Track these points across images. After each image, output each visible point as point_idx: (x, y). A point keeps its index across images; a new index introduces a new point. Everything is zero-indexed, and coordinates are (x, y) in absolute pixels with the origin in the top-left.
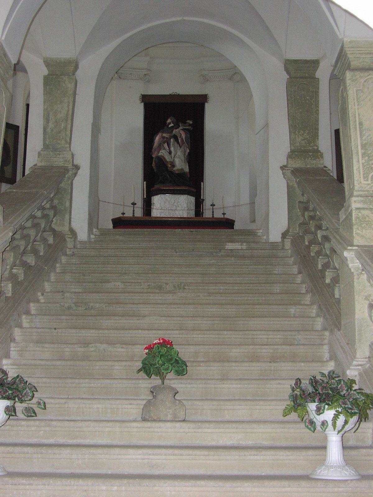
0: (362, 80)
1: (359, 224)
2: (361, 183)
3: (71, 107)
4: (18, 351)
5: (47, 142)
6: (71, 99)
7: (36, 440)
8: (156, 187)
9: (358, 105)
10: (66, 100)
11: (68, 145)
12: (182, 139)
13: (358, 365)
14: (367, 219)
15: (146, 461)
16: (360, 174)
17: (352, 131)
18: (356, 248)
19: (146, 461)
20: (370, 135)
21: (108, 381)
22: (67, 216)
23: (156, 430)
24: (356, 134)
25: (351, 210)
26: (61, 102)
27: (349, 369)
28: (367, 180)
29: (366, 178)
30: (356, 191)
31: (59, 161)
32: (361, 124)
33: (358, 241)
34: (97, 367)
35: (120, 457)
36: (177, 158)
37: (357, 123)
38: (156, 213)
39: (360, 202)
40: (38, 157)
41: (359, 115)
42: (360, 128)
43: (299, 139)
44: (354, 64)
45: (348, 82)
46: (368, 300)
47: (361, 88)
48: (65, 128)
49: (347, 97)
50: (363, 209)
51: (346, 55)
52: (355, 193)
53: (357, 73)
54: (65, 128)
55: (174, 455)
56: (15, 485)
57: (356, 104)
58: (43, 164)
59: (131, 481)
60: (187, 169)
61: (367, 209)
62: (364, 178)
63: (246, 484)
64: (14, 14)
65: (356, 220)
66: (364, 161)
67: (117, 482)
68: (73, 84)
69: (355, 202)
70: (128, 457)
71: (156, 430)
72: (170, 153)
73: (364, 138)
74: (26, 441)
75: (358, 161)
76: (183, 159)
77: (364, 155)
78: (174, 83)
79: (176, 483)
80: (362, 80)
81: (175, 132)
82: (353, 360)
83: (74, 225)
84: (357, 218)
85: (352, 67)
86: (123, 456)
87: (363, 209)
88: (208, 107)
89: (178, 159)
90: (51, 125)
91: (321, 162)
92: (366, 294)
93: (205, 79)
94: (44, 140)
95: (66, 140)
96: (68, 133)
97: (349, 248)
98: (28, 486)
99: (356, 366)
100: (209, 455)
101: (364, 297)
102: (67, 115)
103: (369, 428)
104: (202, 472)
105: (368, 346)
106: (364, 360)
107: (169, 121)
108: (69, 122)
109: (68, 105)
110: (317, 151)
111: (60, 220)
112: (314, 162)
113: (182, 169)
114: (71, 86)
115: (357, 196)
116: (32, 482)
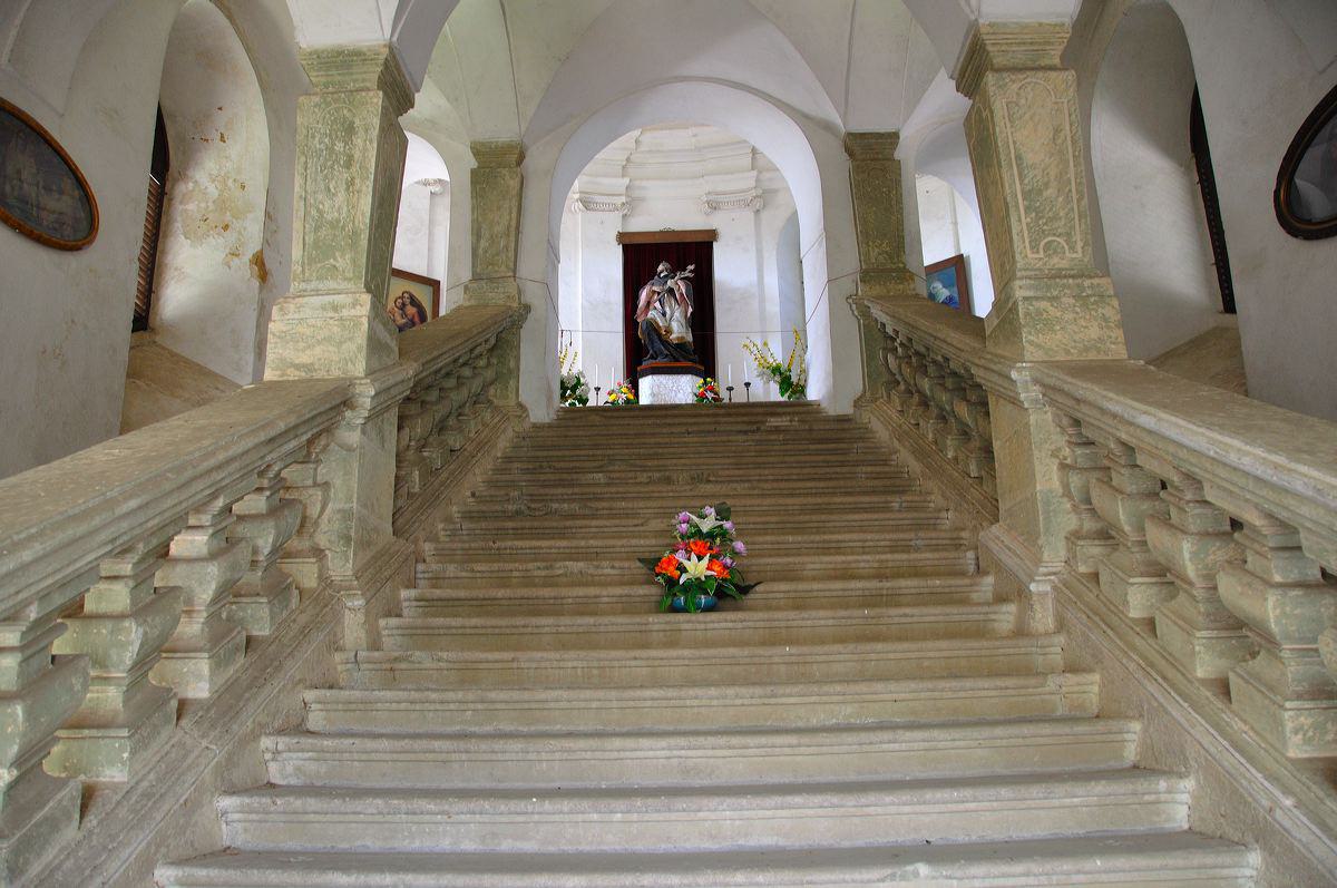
0: (1015, 87)
1: (1031, 324)
2: (1026, 256)
3: (514, 215)
4: (428, 579)
5: (478, 270)
6: (514, 203)
7: (458, 728)
8: (646, 364)
9: (1012, 126)
10: (506, 206)
11: (511, 274)
12: (682, 295)
13: (1050, 574)
14: (1045, 315)
15: (675, 761)
16: (1024, 242)
17: (1004, 170)
18: (1029, 365)
19: (675, 761)
20: (1035, 176)
21: (591, 620)
22: (512, 383)
23: (688, 702)
24: (1012, 175)
25: (1015, 303)
26: (499, 208)
27: (1034, 581)
28: (1038, 252)
29: (1035, 249)
30: (1020, 270)
31: (497, 297)
32: (1019, 158)
33: (1031, 353)
34: (570, 601)
35: (622, 755)
36: (675, 322)
37: (1013, 157)
38: (644, 400)
39: (1030, 287)
40: (465, 293)
41: (1014, 142)
42: (1018, 166)
43: (873, 254)
44: (998, 61)
45: (991, 90)
46: (1058, 457)
47: (1014, 100)
48: (506, 247)
49: (992, 117)
50: (1037, 298)
51: (983, 46)
52: (1019, 274)
53: (1005, 75)
54: (506, 247)
55: (730, 748)
56: (415, 813)
57: (1008, 125)
58: (473, 302)
59: (650, 801)
60: (690, 338)
61: (1043, 298)
62: (1032, 248)
63: (888, 799)
64: (477, 654)
65: (1025, 318)
66: (1029, 220)
67: (621, 804)
68: (518, 180)
69: (1020, 287)
70: (639, 754)
71: (688, 702)
72: (664, 314)
73: (1026, 181)
74: (439, 729)
75: (1020, 220)
76: (684, 322)
77: (1027, 209)
78: (668, 213)
79: (744, 801)
80: (1015, 87)
81: (670, 283)
82: (1037, 566)
83: (523, 398)
84: (1027, 314)
85: (996, 66)
86: (628, 754)
87: (1037, 298)
88: (718, 251)
89: (675, 322)
90: (483, 244)
91: (912, 286)
92: (1053, 447)
93: (714, 206)
94: (474, 266)
95: (507, 266)
96: (511, 254)
97: (1019, 365)
98: (439, 817)
99: (1045, 575)
100: (799, 745)
101: (1050, 453)
102: (509, 227)
103: (1092, 684)
104: (787, 779)
105: (1063, 539)
106: (1058, 564)
107: (661, 268)
108: (513, 238)
109: (511, 213)
110: (905, 270)
111: (501, 390)
112: (901, 286)
113: (683, 338)
114: (514, 184)
115: (1021, 278)
116: (446, 807)
